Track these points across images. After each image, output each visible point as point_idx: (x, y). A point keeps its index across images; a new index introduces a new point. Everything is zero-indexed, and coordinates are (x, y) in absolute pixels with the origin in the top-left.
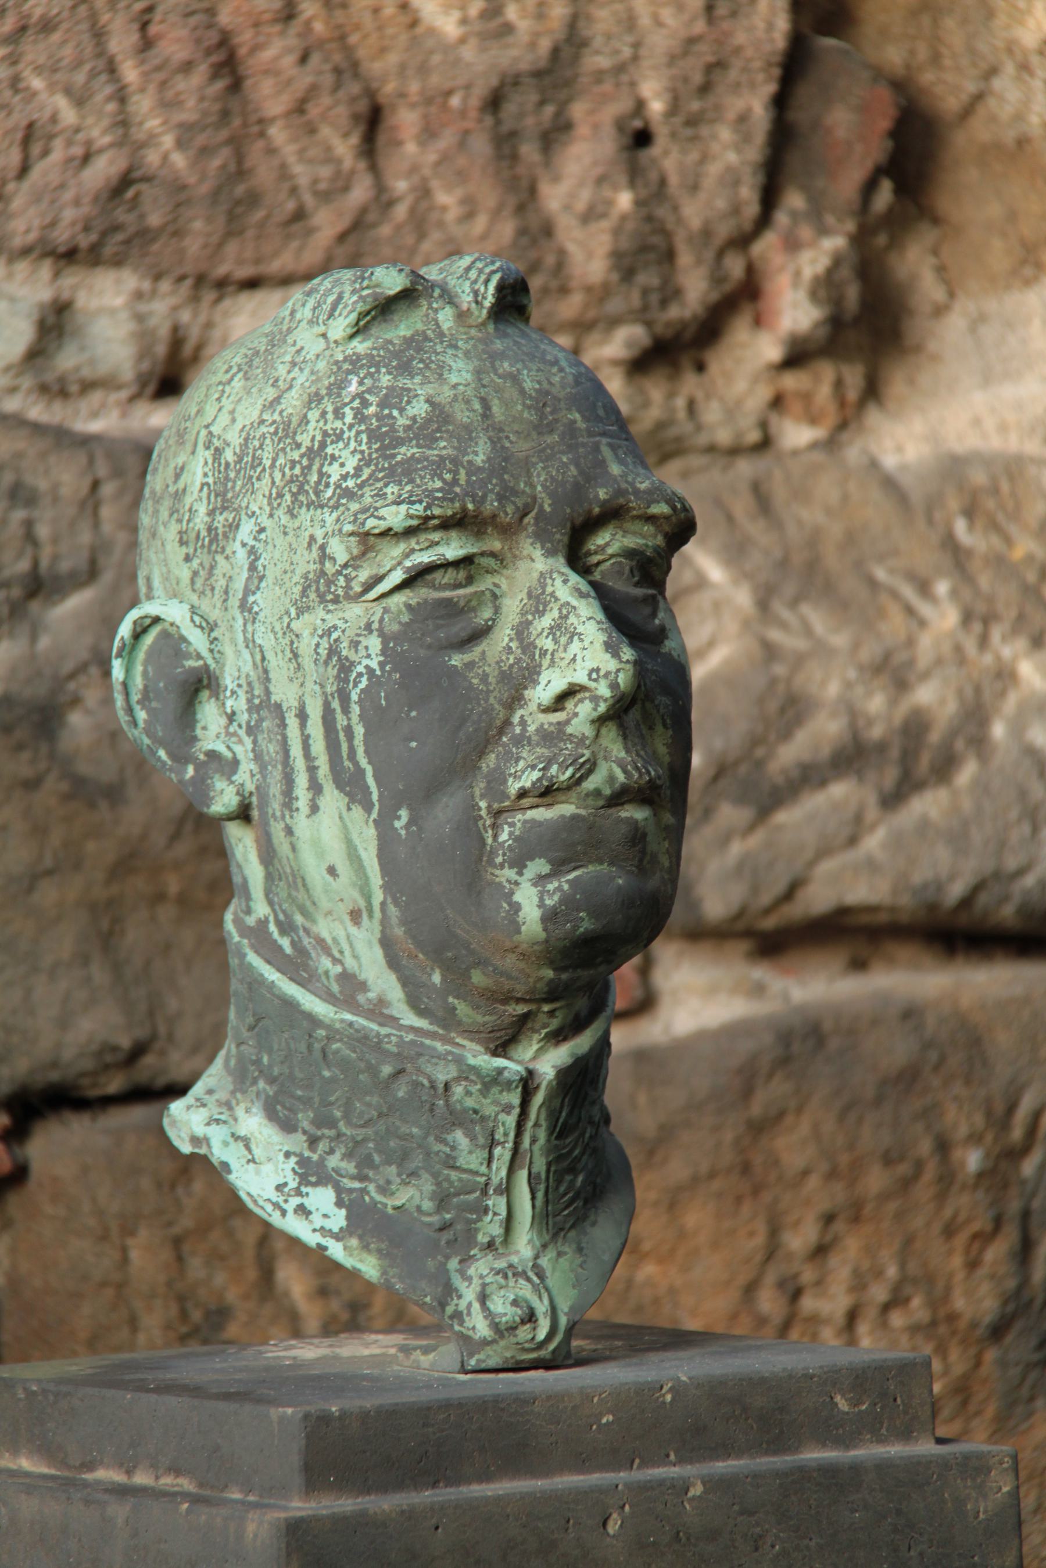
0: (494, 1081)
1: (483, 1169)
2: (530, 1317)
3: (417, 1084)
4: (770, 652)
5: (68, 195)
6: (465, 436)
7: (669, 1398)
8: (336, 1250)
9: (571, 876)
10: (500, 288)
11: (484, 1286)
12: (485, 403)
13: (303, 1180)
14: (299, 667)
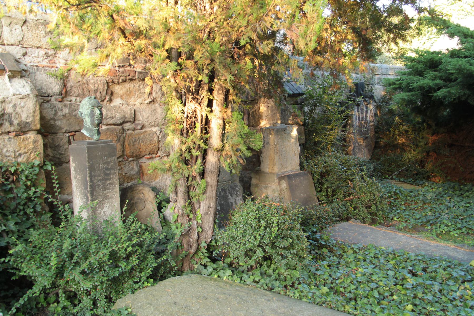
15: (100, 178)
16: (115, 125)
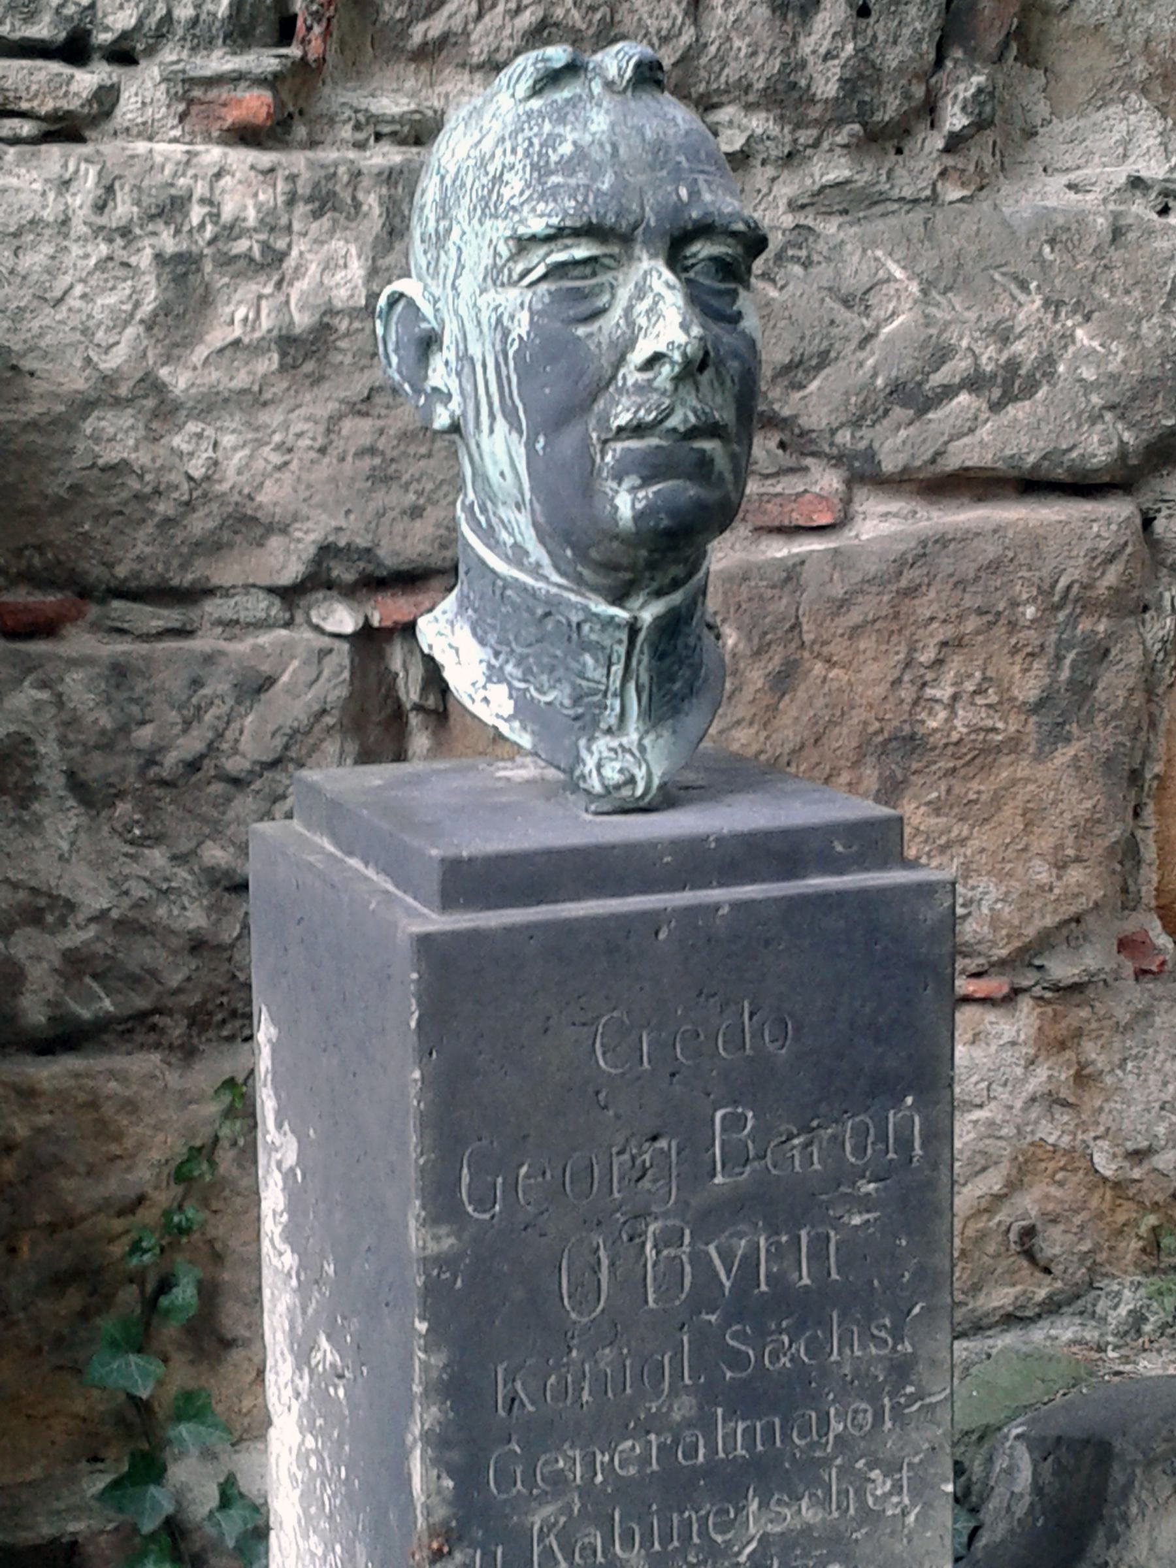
0: (610, 622)
1: (604, 680)
2: (632, 781)
3: (559, 622)
4: (928, 321)
5: (507, 32)
6: (597, 170)
7: (713, 845)
8: (504, 728)
9: (655, 488)
10: (638, 65)
11: (600, 759)
12: (615, 147)
13: (489, 679)
14: (481, 332)
15: (628, 1456)
16: (1031, 485)
